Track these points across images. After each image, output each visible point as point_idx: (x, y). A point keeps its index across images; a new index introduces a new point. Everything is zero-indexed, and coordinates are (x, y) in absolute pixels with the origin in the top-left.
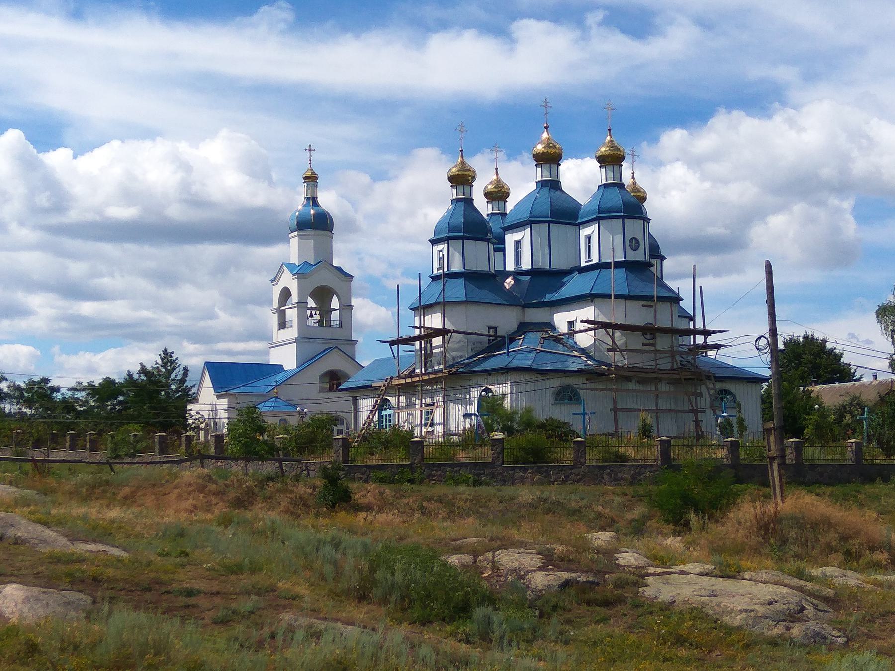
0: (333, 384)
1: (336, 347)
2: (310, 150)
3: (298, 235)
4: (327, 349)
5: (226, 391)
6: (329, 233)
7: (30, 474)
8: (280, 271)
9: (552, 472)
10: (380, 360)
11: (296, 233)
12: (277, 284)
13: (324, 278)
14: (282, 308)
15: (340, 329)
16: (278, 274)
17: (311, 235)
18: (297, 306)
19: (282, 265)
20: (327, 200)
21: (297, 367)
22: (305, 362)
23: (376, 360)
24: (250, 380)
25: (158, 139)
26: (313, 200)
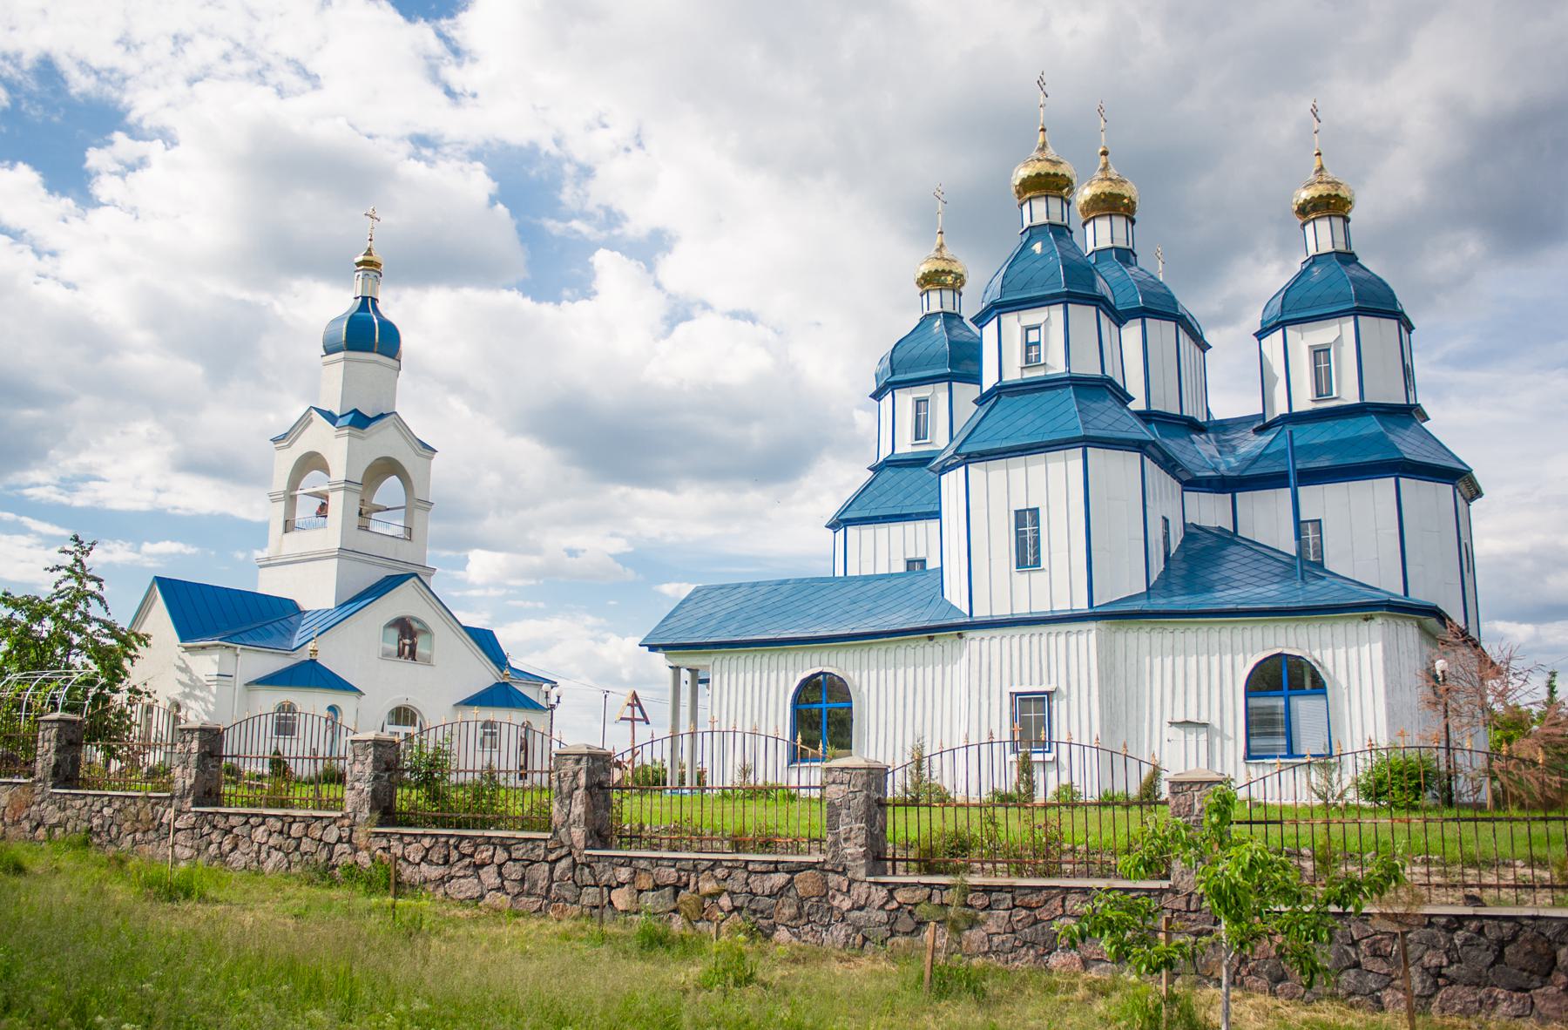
0: (404, 645)
11: (341, 355)
14: (293, 493)
18: (345, 489)
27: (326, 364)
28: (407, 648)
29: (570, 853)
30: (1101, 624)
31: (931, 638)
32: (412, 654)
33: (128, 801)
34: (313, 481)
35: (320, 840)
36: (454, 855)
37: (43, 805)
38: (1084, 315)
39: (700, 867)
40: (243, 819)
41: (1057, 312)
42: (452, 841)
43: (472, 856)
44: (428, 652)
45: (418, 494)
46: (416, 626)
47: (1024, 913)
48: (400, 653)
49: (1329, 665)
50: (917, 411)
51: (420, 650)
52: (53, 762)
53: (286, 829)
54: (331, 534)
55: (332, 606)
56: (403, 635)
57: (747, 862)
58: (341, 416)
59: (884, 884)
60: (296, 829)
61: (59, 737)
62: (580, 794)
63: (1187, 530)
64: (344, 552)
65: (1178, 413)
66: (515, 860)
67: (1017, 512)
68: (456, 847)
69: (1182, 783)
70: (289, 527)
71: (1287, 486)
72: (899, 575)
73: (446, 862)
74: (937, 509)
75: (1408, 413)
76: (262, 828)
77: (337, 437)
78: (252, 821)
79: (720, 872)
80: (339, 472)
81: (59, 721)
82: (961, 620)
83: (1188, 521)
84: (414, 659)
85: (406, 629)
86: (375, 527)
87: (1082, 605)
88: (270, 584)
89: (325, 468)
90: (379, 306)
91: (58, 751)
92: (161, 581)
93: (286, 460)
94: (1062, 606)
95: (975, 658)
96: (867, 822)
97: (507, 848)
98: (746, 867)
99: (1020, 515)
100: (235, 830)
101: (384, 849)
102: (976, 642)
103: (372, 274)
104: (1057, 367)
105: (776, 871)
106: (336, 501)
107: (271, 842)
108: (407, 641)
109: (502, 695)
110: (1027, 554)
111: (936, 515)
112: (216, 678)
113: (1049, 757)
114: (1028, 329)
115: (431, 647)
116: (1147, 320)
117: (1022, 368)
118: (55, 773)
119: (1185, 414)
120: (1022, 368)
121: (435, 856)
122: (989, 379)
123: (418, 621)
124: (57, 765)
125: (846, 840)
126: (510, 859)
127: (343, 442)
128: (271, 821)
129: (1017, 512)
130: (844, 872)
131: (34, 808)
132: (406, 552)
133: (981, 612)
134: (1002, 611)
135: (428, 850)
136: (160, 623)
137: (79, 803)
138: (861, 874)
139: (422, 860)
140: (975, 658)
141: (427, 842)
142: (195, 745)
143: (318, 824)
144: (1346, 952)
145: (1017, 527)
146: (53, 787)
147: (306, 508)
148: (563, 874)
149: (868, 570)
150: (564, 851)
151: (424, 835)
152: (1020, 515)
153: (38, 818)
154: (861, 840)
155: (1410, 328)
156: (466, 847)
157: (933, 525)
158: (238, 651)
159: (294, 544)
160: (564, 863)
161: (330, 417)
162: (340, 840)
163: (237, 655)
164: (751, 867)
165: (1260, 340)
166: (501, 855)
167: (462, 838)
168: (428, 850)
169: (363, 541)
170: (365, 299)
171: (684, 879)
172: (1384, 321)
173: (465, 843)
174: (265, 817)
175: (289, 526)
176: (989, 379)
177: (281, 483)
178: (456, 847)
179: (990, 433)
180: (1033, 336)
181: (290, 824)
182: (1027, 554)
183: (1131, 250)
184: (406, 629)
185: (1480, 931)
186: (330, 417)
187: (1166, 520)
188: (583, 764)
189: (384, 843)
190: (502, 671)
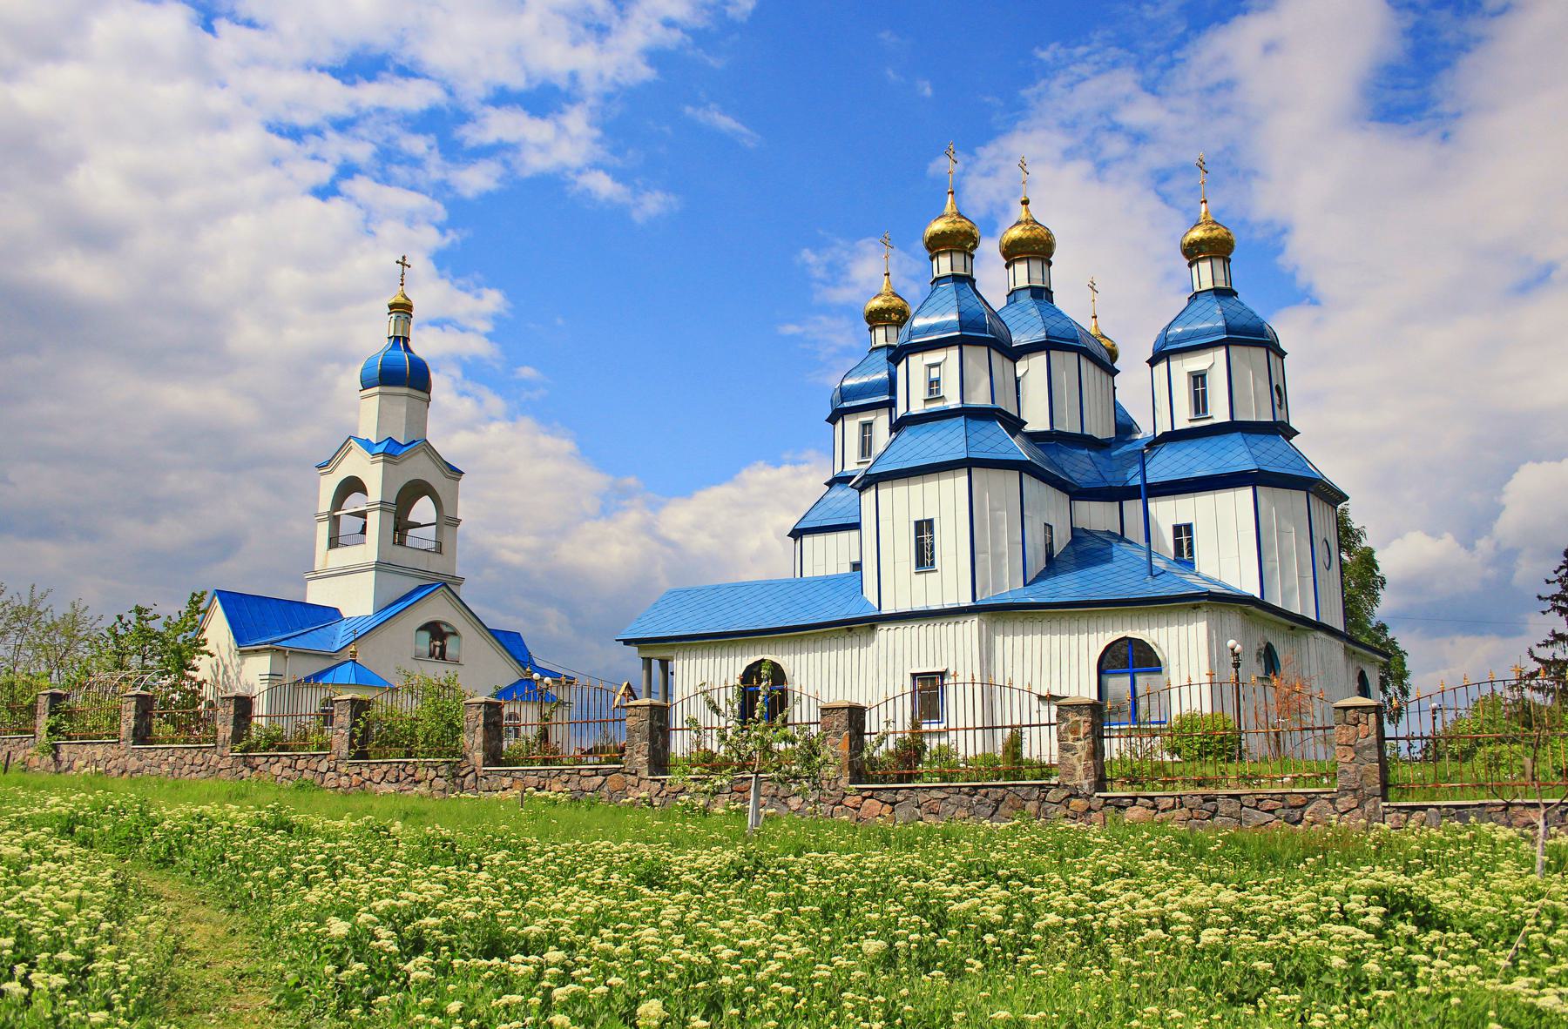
0: (435, 646)
1: (445, 584)
2: (403, 265)
3: (380, 393)
4: (420, 588)
5: (272, 643)
6: (423, 395)
7: (1261, 943)
8: (344, 448)
9: (1212, 848)
10: (1131, 640)
11: (376, 389)
12: (331, 472)
13: (417, 468)
14: (337, 513)
15: (438, 555)
16: (337, 453)
17: (408, 395)
18: (381, 509)
19: (350, 438)
20: (424, 344)
21: (377, 612)
22: (391, 609)
23: (1125, 638)
24: (292, 631)
25: (357, 176)
26: (401, 341)
27: (363, 398)
28: (438, 649)
29: (474, 770)
30: (983, 616)
31: (850, 630)
32: (442, 655)
33: (186, 751)
34: (354, 502)
35: (316, 771)
36: (403, 775)
37: (127, 758)
38: (977, 357)
39: (552, 775)
40: (266, 759)
41: (953, 353)
42: (401, 766)
43: (413, 775)
44: (456, 652)
45: (447, 512)
46: (445, 629)
47: (738, 794)
48: (432, 654)
49: (1163, 645)
50: (864, 433)
51: (449, 651)
52: (133, 726)
53: (293, 765)
54: (369, 550)
55: (371, 612)
56: (434, 637)
57: (580, 770)
58: (377, 444)
59: (659, 780)
60: (301, 764)
61: (137, 708)
62: (480, 729)
63: (1076, 534)
64: (381, 566)
65: (1079, 432)
66: (441, 777)
67: (917, 523)
68: (404, 770)
69: (827, 709)
70: (333, 544)
71: (1139, 497)
72: (845, 576)
73: (397, 781)
74: (856, 520)
75: (1282, 430)
76: (278, 765)
77: (373, 463)
78: (271, 760)
79: (564, 777)
80: (375, 493)
81: (136, 696)
82: (872, 614)
83: (1079, 525)
84: (444, 659)
85: (436, 631)
86: (409, 541)
87: (966, 601)
88: (317, 594)
89: (363, 490)
90: (411, 344)
91: (136, 718)
92: (220, 593)
93: (329, 485)
94: (950, 602)
95: (883, 645)
96: (650, 740)
97: (436, 768)
98: (579, 773)
99: (919, 525)
100: (259, 768)
101: (358, 774)
102: (884, 633)
103: (403, 316)
104: (953, 402)
105: (597, 775)
106: (374, 519)
107: (284, 775)
108: (438, 643)
109: (524, 689)
110: (924, 558)
111: (856, 526)
112: (267, 677)
113: (942, 726)
114: (931, 366)
115: (459, 649)
116: (1052, 352)
117: (925, 400)
118: (135, 735)
119: (1086, 432)
120: (925, 400)
121: (390, 777)
122: (901, 410)
123: (447, 625)
124: (136, 729)
125: (637, 752)
126: (437, 776)
127: (379, 467)
128: (284, 758)
129: (917, 523)
130: (635, 774)
131: (120, 760)
132: (436, 564)
133: (887, 609)
134: (904, 607)
135: (386, 773)
136: (218, 629)
137: (151, 755)
138: (645, 774)
139: (382, 780)
140: (883, 645)
141: (385, 768)
142: (232, 709)
143: (315, 760)
144: (915, 812)
145: (916, 535)
146: (133, 744)
147: (349, 525)
148: (469, 784)
149: (820, 573)
150: (470, 769)
151: (383, 763)
152: (919, 525)
153: (123, 767)
154: (646, 752)
155: (1282, 354)
156: (410, 769)
157: (854, 534)
158: (287, 654)
159: (341, 557)
160: (470, 777)
161: (367, 445)
162: (328, 770)
163: (286, 657)
164: (582, 773)
165: (1152, 366)
166: (432, 773)
167: (407, 763)
168: (386, 773)
169: (399, 555)
170: (397, 338)
171: (542, 783)
172: (1253, 350)
173: (408, 767)
174: (279, 756)
175: (334, 543)
176: (901, 410)
177: (325, 505)
178: (404, 770)
179: (894, 457)
180: (935, 373)
181: (296, 761)
182: (924, 558)
183: (1046, 289)
184: (436, 631)
185: (986, 795)
186: (367, 445)
187: (1049, 527)
188: (482, 710)
189: (358, 771)
190: (525, 669)
